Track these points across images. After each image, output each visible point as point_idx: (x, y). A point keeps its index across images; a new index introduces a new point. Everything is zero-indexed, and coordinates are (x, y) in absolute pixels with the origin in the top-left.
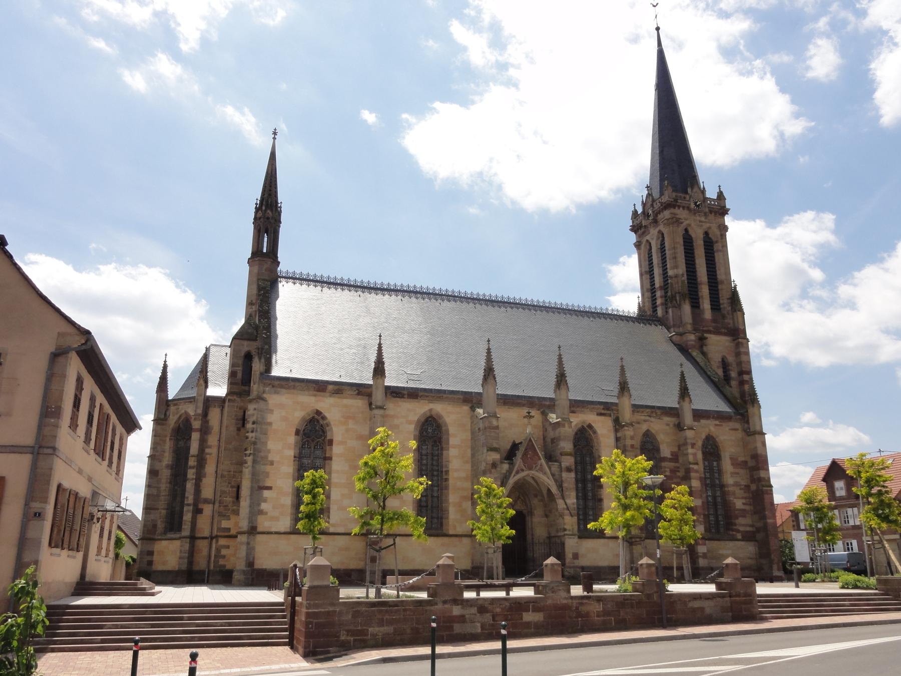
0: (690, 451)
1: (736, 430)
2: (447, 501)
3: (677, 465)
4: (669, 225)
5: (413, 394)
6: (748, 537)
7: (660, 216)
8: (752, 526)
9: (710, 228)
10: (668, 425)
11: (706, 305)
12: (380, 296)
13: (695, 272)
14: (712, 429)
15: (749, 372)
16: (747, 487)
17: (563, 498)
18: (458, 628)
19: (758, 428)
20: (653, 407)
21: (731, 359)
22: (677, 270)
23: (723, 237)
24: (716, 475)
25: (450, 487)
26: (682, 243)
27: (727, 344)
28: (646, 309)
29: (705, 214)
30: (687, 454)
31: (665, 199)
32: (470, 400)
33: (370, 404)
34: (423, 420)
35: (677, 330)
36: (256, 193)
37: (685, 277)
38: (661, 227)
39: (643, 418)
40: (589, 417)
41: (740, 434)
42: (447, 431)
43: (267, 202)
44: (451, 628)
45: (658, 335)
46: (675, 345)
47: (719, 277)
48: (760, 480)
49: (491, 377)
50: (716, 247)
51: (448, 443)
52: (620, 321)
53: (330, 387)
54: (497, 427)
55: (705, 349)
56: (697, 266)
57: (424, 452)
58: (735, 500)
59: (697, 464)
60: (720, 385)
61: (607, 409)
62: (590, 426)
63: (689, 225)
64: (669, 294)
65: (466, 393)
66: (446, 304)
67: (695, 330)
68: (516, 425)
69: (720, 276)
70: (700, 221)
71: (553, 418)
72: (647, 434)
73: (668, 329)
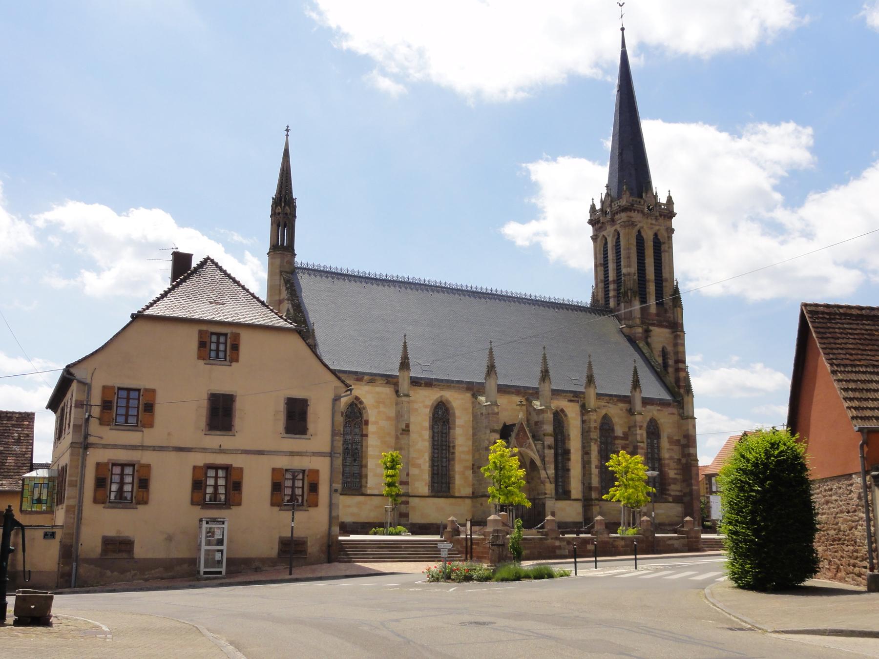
0: (639, 432)
1: (673, 414)
2: (454, 470)
3: (627, 442)
4: (625, 227)
5: (429, 383)
6: (677, 500)
7: (617, 217)
8: (681, 491)
9: (658, 230)
10: (622, 410)
11: (652, 301)
12: (380, 288)
13: (644, 270)
14: (655, 413)
15: (684, 362)
16: (679, 460)
17: (545, 469)
18: (558, 552)
19: (691, 414)
20: (611, 395)
21: (670, 349)
22: (630, 269)
23: (670, 238)
24: (656, 451)
25: (457, 459)
26: (635, 244)
27: (668, 335)
28: (599, 298)
29: (656, 219)
30: (636, 434)
31: (623, 202)
32: (474, 389)
33: (397, 392)
34: (435, 404)
35: (627, 322)
36: (272, 191)
37: (636, 277)
38: (617, 227)
39: (603, 404)
40: (561, 403)
41: (676, 418)
42: (454, 413)
43: (285, 198)
44: (555, 552)
45: (609, 326)
46: (625, 336)
47: (664, 275)
48: (689, 455)
49: (493, 372)
50: (663, 247)
51: (454, 424)
52: (579, 312)
53: (366, 377)
54: (497, 414)
55: (649, 340)
56: (647, 265)
57: (436, 431)
58: (669, 471)
59: (643, 442)
60: (660, 376)
61: (576, 396)
62: (562, 411)
63: (642, 227)
64: (622, 290)
65: (469, 383)
66: (436, 295)
67: (643, 323)
68: (510, 409)
69: (665, 275)
70: (652, 224)
71: (537, 404)
72: (606, 417)
73: (620, 320)
